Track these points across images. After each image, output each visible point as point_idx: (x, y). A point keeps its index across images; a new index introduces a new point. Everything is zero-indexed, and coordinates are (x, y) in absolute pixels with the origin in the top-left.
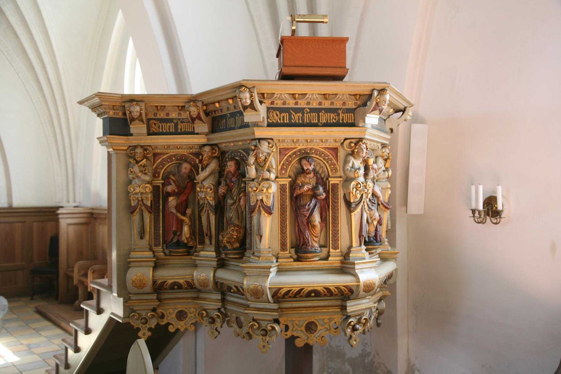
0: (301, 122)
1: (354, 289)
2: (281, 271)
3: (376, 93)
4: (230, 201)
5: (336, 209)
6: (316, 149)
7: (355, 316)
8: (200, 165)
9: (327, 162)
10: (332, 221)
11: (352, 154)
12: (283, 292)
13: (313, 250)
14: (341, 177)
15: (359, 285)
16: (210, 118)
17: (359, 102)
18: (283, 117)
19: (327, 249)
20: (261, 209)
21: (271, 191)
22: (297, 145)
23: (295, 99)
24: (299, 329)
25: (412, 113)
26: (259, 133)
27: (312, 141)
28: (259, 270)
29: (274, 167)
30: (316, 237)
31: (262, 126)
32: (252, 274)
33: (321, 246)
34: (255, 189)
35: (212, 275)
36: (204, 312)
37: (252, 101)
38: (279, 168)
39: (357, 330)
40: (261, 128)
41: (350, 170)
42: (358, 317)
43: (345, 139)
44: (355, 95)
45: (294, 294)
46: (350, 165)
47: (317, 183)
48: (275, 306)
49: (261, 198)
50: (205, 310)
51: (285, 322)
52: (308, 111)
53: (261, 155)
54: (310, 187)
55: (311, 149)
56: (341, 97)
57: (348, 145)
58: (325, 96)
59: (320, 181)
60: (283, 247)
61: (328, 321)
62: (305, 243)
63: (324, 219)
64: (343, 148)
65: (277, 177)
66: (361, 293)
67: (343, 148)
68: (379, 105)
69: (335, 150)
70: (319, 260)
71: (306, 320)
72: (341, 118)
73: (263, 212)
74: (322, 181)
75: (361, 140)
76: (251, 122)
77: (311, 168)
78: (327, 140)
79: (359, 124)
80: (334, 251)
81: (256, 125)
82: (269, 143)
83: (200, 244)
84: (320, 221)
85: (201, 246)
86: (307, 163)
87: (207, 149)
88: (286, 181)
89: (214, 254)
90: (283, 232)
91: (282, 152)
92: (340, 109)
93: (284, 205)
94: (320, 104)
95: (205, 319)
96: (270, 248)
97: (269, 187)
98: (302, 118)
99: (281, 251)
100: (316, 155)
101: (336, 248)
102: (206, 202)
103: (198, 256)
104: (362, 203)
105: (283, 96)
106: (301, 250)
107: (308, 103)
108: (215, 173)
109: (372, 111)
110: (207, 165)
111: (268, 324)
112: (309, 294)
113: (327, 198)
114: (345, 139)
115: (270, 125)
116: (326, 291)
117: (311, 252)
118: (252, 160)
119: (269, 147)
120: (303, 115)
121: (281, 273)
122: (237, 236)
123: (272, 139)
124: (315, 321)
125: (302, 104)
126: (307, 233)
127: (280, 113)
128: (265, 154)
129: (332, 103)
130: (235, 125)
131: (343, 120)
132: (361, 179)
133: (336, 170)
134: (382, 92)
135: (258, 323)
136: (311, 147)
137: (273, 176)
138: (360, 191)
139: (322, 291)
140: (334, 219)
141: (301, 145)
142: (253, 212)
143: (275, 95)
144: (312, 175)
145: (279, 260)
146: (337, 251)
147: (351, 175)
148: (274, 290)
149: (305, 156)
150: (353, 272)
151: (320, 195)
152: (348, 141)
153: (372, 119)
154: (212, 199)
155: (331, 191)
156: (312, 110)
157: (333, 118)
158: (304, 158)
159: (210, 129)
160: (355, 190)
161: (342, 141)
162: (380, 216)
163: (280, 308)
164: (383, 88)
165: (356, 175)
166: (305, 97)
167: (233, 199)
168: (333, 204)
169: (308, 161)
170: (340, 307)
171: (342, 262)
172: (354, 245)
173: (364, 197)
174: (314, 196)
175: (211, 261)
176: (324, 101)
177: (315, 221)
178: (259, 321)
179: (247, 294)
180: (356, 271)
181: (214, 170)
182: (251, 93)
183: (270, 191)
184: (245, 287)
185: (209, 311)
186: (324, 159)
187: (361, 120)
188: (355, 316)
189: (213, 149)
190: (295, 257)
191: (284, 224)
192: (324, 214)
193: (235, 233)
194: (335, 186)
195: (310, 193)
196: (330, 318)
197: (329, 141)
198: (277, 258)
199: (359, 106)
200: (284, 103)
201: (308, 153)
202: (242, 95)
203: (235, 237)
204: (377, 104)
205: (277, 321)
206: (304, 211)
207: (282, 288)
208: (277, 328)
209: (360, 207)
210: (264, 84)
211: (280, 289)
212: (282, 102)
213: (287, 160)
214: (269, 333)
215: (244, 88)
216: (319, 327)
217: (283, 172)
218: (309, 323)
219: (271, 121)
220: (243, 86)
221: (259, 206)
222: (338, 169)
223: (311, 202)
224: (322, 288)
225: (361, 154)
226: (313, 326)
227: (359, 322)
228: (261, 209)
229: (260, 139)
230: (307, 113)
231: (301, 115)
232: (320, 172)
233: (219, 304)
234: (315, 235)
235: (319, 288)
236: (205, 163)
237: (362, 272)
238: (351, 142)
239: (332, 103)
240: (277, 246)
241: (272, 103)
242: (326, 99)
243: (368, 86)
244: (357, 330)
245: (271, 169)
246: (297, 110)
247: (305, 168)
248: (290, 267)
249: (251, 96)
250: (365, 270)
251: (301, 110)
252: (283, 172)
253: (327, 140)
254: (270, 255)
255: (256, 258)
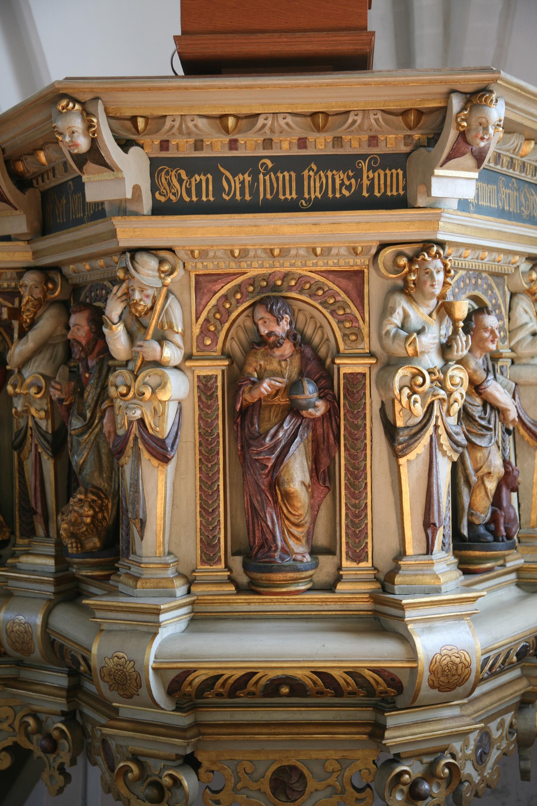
0: (248, 198)
1: (405, 680)
2: (201, 619)
3: (456, 103)
4: (76, 424)
5: (360, 445)
6: (301, 277)
7: (418, 756)
8: (16, 324)
9: (333, 313)
10: (347, 479)
11: (404, 289)
12: (199, 678)
13: (288, 561)
14: (371, 355)
15: (416, 667)
16: (33, 195)
17: (417, 135)
18: (199, 186)
19: (335, 559)
20: (141, 446)
21: (171, 396)
22: (244, 265)
23: (227, 130)
24: (255, 786)
25: (484, 147)
26: (130, 233)
27: (284, 252)
28: (131, 616)
29: (179, 329)
30: (297, 525)
31: (136, 214)
32: (115, 627)
33: (314, 552)
34: (123, 390)
35: (39, 620)
36: (31, 721)
37: (94, 141)
38: (197, 330)
39: (423, 797)
40: (133, 218)
41: (396, 335)
42: (427, 760)
43: (383, 246)
44: (405, 113)
45: (228, 686)
46: (397, 319)
47: (301, 374)
48: (183, 720)
49: (138, 414)
50: (34, 715)
51: (214, 763)
52: (270, 164)
53: (137, 296)
54: (279, 383)
55: (286, 276)
56: (359, 119)
57: (389, 263)
58: (317, 119)
59: (312, 366)
60: (208, 550)
61: (337, 766)
62: (267, 544)
63: (322, 473)
64: (377, 270)
65: (188, 357)
66: (422, 693)
67: (377, 270)
68: (469, 138)
69: (355, 279)
70: (309, 590)
71: (274, 761)
72: (366, 182)
73: (145, 455)
74: (318, 367)
75: (427, 245)
76: (111, 202)
77: (282, 328)
78: (330, 249)
79: (416, 200)
80: (354, 565)
81: (123, 209)
82: (161, 261)
83: (23, 535)
84: (307, 480)
85: (26, 541)
86: (267, 316)
87: (30, 279)
88: (215, 368)
89: (51, 562)
90: (207, 510)
91: (203, 284)
92: (364, 157)
93: (211, 434)
94: (302, 143)
95: (35, 738)
96: (170, 553)
97: (162, 385)
98: (251, 187)
99: (203, 562)
100: (301, 292)
101: (358, 556)
102: (31, 424)
103: (14, 568)
104: (431, 430)
105: (191, 124)
106: (256, 563)
107: (268, 143)
108: (54, 345)
109: (449, 158)
110: (33, 323)
111: (165, 768)
112: (273, 688)
113: (332, 413)
114: (383, 246)
115: (159, 210)
116: (320, 682)
117: (281, 569)
118: (114, 309)
119: (159, 270)
120: (255, 179)
121: (202, 625)
122: (94, 517)
123: (170, 250)
124: (298, 764)
125: (249, 146)
126: (270, 516)
127: (190, 175)
128: (150, 292)
129: (338, 141)
130: (84, 212)
131: (371, 189)
132: (432, 360)
133: (358, 333)
134: (476, 100)
135: (141, 765)
136: (284, 270)
137: (171, 353)
138: (424, 396)
139: (309, 682)
140: (352, 474)
141: (255, 264)
142: (121, 452)
143: (168, 123)
144: (287, 348)
145: (193, 589)
146: (363, 564)
147: (398, 349)
148: (172, 675)
149: (269, 295)
150: (401, 631)
151: (306, 408)
152: (388, 252)
153: (453, 184)
154: (43, 414)
155: (341, 397)
156: (282, 163)
157: (342, 184)
158: (261, 302)
159: (36, 224)
160: (406, 391)
161: (374, 251)
162: (506, 463)
163: (197, 725)
164: (482, 85)
165: (410, 350)
166: (254, 125)
167: (84, 416)
168: (350, 435)
169: (271, 311)
170: (368, 729)
171: (373, 597)
172: (410, 550)
173: (436, 412)
174: (294, 410)
175: (42, 582)
176: (312, 136)
177: (291, 480)
178: (142, 759)
179: (101, 683)
180: (410, 627)
181: (50, 337)
182: (87, 115)
183: (163, 396)
184: (95, 662)
185: (43, 717)
186: (324, 304)
187: (422, 189)
188: (418, 756)
189: (48, 279)
190: (243, 579)
191: (210, 487)
192: (325, 461)
193: (88, 511)
194: (355, 381)
195: (282, 400)
196: (344, 758)
197: (334, 251)
198: (190, 582)
199: (418, 146)
200: (198, 145)
201: (275, 288)
202: (60, 124)
203: (88, 520)
204: (463, 135)
205: (191, 762)
206: (259, 453)
207: (195, 670)
208: (185, 783)
209: (425, 440)
210: (123, 90)
211: (188, 672)
212: (192, 141)
213: (217, 308)
214: (168, 794)
215: (64, 103)
216: (312, 784)
217: (208, 342)
218: (281, 770)
219: (163, 199)
220: (64, 96)
221: (136, 439)
222: (365, 331)
223: (281, 426)
224: (307, 673)
225: (428, 288)
226: (295, 779)
227: (430, 774)
228: (141, 446)
229: (134, 251)
230: (267, 171)
231: (248, 178)
232: (316, 340)
233: (59, 700)
234: (292, 519)
235: (299, 674)
236: (26, 317)
237: (430, 629)
238: (400, 254)
239: (338, 141)
240: (190, 548)
241: (164, 145)
242: (319, 129)
243: (431, 82)
244: (423, 797)
245: (169, 334)
246: (238, 165)
247: (264, 331)
248: (227, 608)
249: (89, 126)
250: (437, 624)
251: (250, 164)
252: (208, 342)
253: (330, 249)
254: (170, 573)
255: (131, 582)
